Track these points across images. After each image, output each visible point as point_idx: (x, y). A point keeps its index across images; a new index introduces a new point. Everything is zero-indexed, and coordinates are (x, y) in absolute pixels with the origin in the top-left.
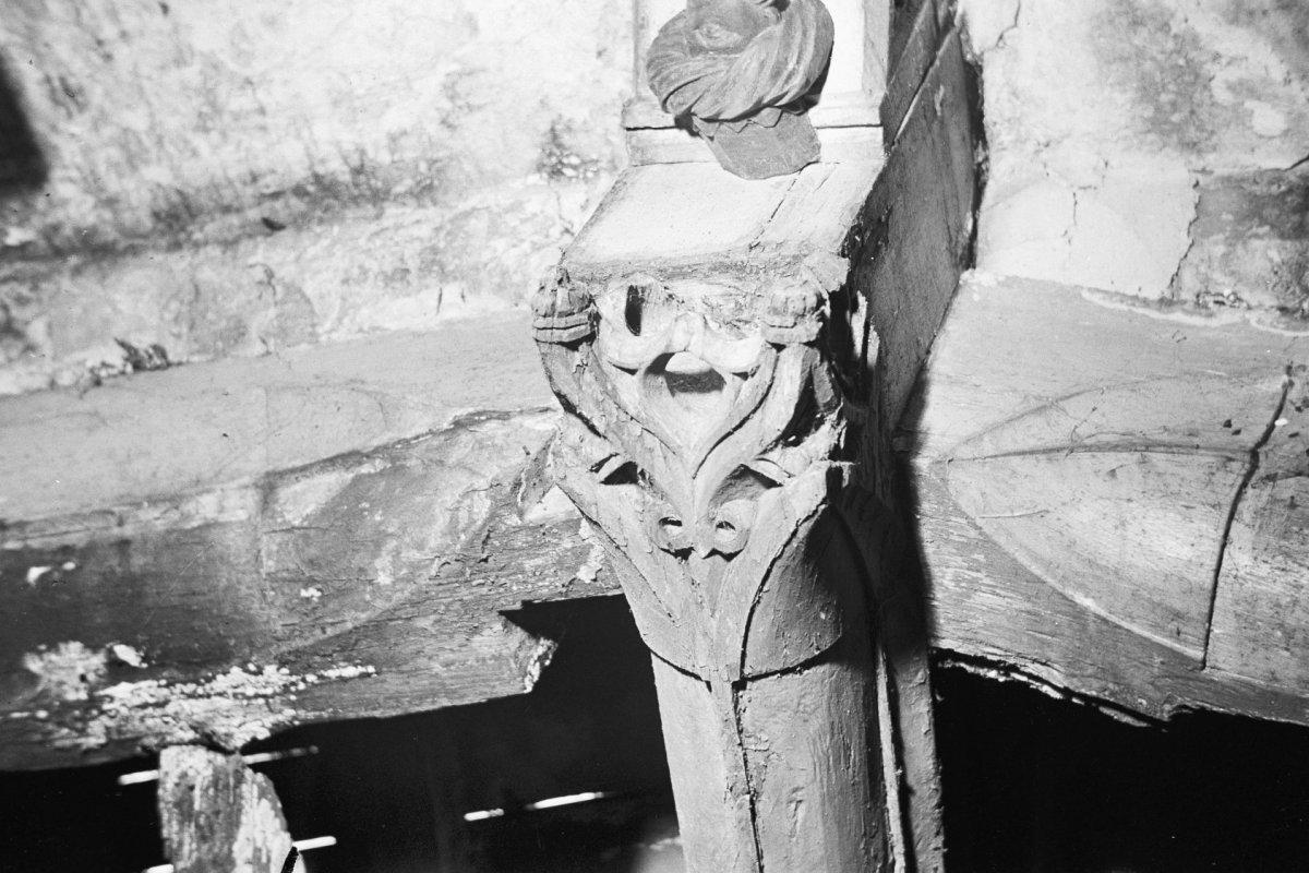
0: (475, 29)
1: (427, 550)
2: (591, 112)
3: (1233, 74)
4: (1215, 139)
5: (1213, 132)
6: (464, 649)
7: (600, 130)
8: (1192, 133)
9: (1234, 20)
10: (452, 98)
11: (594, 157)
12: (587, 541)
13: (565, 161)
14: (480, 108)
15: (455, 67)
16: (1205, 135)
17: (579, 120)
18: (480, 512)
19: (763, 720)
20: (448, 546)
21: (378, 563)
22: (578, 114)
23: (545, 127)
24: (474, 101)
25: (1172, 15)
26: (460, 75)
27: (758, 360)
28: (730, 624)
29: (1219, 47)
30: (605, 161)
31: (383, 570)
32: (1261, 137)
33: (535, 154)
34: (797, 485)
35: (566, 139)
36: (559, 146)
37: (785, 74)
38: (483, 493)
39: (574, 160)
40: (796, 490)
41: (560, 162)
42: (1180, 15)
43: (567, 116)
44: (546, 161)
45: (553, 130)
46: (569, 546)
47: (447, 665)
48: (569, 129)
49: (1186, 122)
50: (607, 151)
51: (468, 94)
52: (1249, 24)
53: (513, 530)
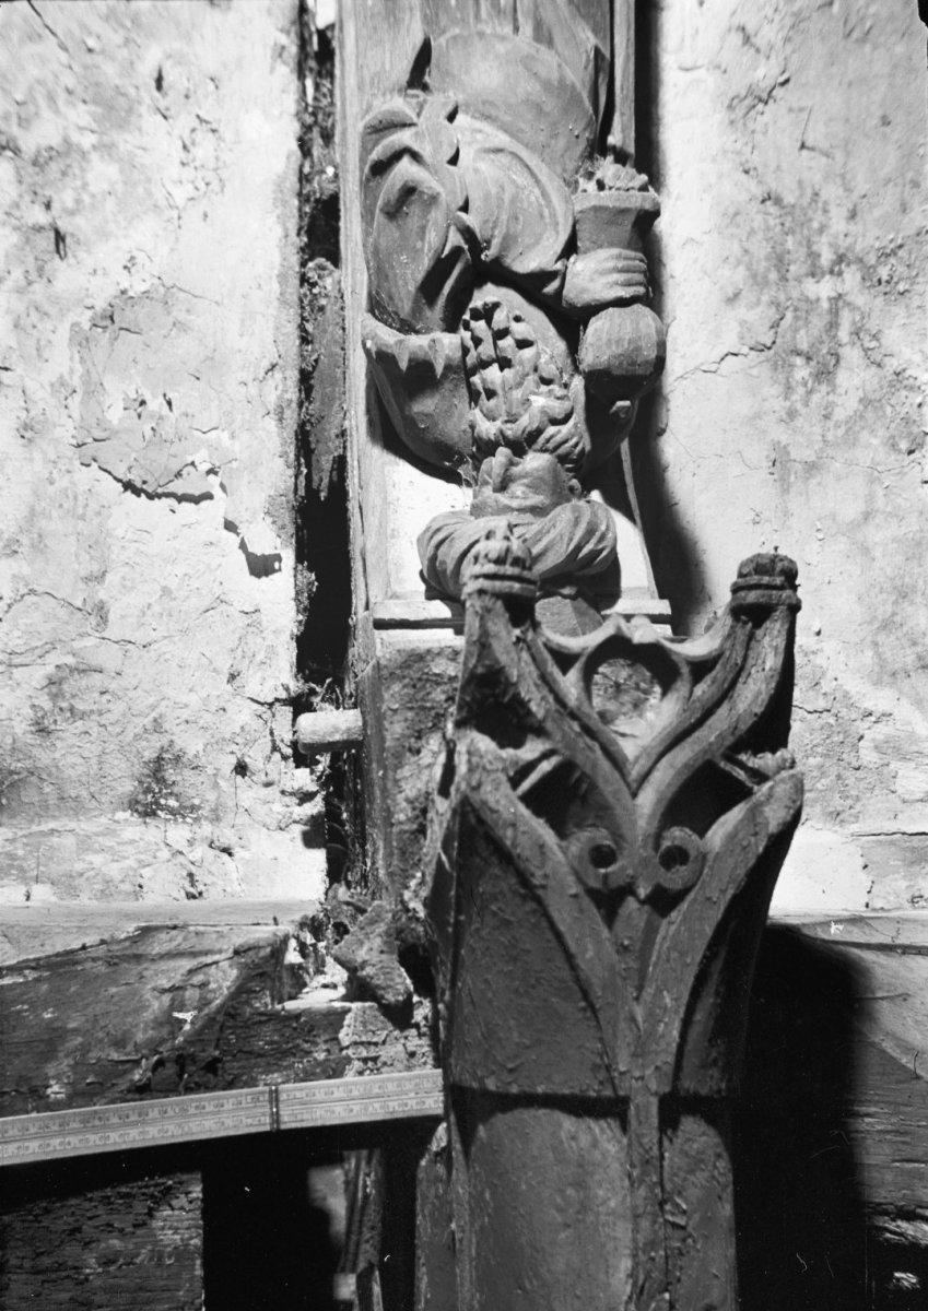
0: (104, 620)
1: (130, 1048)
2: (206, 745)
3: (880, 732)
4: (858, 807)
5: (858, 799)
6: (140, 1232)
7: (210, 770)
8: (837, 802)
9: (878, 683)
10: (54, 697)
11: (196, 802)
12: (344, 1052)
13: (162, 801)
14: (83, 715)
15: (70, 660)
16: (849, 802)
17: (191, 752)
18: (220, 988)
19: (682, 1174)
20: (163, 1041)
21: (51, 1069)
22: (192, 744)
23: (150, 754)
24: (80, 706)
25: (824, 673)
26: (73, 670)
27: (722, 645)
28: (668, 1000)
29: (868, 705)
30: (208, 808)
31: (58, 1078)
32: (904, 802)
33: (128, 787)
34: (771, 788)
35: (170, 774)
36: (161, 781)
37: (598, 534)
38: (226, 963)
39: (172, 803)
40: (770, 796)
41: (157, 803)
42: (830, 674)
43: (179, 744)
44: (141, 797)
45: (159, 759)
46: (321, 1056)
47: (107, 1261)
48: (178, 759)
49: (830, 789)
50: (211, 796)
51: (73, 696)
52: (892, 685)
53: (258, 1018)
